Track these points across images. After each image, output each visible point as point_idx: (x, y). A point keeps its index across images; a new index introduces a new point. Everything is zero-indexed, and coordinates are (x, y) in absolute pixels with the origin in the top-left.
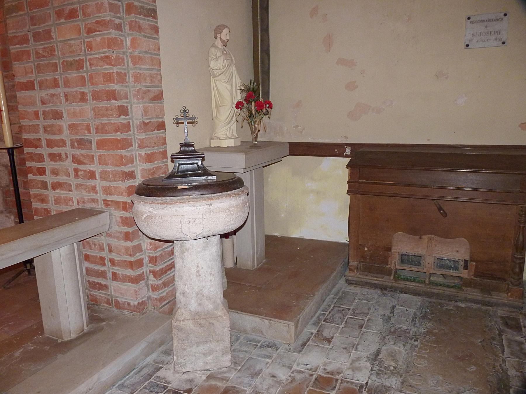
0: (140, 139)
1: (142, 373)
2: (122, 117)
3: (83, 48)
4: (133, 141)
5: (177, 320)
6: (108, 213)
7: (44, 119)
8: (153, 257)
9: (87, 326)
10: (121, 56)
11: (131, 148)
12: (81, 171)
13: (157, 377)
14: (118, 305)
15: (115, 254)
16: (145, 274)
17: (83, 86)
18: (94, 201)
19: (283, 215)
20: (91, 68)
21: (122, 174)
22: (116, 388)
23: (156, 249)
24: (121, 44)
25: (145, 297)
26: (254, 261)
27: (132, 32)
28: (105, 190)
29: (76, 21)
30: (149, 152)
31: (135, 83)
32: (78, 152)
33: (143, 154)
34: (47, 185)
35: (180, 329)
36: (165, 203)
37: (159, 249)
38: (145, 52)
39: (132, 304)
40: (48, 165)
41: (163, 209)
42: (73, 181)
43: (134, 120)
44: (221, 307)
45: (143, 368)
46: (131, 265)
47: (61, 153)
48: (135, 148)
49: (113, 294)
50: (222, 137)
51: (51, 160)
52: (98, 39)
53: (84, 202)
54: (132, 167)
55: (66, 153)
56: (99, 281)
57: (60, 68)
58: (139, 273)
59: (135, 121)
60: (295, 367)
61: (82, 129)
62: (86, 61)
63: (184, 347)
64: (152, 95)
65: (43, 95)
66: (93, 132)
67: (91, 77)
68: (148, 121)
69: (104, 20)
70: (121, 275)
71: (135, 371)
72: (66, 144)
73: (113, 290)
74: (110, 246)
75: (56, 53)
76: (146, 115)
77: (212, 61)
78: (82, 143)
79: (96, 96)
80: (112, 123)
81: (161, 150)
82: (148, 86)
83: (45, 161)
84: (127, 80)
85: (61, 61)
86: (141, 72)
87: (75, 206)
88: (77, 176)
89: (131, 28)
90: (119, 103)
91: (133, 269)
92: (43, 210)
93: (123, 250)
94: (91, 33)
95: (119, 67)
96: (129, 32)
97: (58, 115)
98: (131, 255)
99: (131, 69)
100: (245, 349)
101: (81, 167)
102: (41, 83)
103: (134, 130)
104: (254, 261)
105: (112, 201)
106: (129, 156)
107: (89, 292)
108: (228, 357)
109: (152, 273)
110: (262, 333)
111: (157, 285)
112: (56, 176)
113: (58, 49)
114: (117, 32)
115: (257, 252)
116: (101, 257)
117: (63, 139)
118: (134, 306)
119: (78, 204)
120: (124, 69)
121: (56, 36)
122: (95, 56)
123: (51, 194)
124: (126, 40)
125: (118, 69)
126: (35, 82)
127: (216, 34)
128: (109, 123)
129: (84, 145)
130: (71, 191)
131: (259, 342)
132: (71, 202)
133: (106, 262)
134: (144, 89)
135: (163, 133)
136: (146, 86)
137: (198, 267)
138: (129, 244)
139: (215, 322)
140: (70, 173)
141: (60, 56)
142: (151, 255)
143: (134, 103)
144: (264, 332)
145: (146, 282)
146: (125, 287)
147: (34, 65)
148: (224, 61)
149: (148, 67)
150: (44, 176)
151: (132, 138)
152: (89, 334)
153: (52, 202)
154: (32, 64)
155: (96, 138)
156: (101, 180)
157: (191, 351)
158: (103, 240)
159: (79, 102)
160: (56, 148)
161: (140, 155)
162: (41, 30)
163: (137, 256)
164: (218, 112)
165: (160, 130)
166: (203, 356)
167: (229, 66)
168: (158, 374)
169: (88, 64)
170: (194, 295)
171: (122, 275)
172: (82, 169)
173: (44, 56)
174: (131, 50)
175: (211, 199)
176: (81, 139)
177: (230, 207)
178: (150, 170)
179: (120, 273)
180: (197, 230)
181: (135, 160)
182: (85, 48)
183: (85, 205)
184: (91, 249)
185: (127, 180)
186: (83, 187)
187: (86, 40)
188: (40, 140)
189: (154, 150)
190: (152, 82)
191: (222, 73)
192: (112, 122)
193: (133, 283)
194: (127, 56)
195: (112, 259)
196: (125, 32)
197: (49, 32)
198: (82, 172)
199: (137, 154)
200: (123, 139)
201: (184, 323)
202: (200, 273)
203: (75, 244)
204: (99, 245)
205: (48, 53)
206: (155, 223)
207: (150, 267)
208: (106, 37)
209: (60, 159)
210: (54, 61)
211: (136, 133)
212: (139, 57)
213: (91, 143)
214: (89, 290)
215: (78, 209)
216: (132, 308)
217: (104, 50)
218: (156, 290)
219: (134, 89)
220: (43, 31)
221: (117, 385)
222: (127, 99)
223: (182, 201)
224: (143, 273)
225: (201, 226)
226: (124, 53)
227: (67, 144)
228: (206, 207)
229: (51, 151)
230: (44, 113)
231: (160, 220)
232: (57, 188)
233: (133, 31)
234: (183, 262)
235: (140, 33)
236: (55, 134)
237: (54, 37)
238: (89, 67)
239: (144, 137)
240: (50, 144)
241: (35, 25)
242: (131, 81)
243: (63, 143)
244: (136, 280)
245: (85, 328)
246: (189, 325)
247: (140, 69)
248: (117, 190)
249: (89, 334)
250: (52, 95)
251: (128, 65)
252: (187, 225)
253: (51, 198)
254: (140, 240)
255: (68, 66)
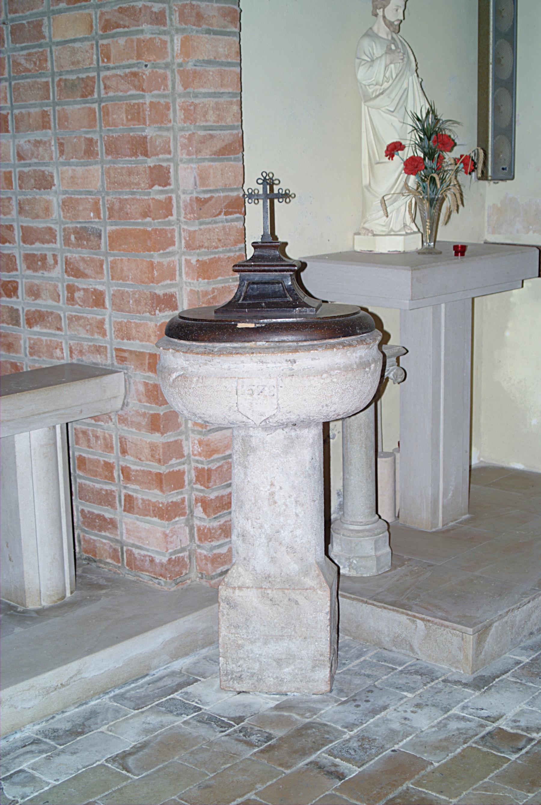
0: (190, 232)
1: (160, 684)
2: (156, 187)
3: (95, 57)
4: (176, 234)
5: (227, 585)
6: (122, 373)
7: (21, 187)
8: (203, 469)
9: (72, 593)
10: (161, 71)
11: (170, 249)
12: (79, 290)
13: (186, 693)
14: (133, 563)
15: (132, 459)
16: (186, 503)
17: (91, 127)
18: (99, 350)
19: (534, 421)
20: (107, 93)
21: (152, 299)
22: (110, 698)
23: (211, 455)
24: (161, 50)
25: (183, 550)
26: (435, 512)
27: (184, 26)
28: (120, 330)
29: (86, 7)
30: (205, 258)
31: (185, 122)
32: (75, 255)
33: (193, 261)
34: (18, 316)
35: (232, 605)
36: (209, 353)
37: (215, 456)
38: (209, 62)
39: (157, 561)
40: (23, 276)
41: (206, 364)
42: (64, 310)
43: (180, 192)
44: (315, 571)
45: (164, 677)
46: (159, 480)
47: (46, 255)
48: (180, 248)
49: (124, 538)
50: (378, 229)
51: (28, 268)
52: (122, 41)
53: (81, 352)
54: (171, 286)
55: (54, 256)
56: (102, 513)
57: (54, 93)
58: (174, 500)
59: (182, 196)
60: (456, 711)
61: (85, 209)
62: (99, 81)
63: (240, 642)
64: (218, 145)
65: (22, 142)
66: (105, 216)
67: (106, 112)
68: (207, 196)
69: (133, 7)
70: (140, 501)
71: (147, 679)
72: (55, 239)
73: (124, 531)
74: (123, 442)
75: (49, 64)
76: (203, 184)
77: (361, 68)
78: (84, 236)
79: (112, 148)
80: (137, 200)
81: (232, 254)
82: (211, 128)
83: (17, 270)
84: (171, 116)
85: (57, 79)
86: (197, 101)
87: (66, 359)
88: (71, 300)
89: (183, 18)
90: (151, 162)
91: (162, 490)
92: (9, 366)
93: (147, 451)
94: (110, 30)
95: (156, 92)
96: (178, 26)
97: (44, 182)
98: (159, 461)
99: (180, 96)
100: (368, 672)
101: (80, 283)
102: (18, 120)
103: (179, 214)
104: (435, 512)
105: (131, 352)
106: (165, 264)
107: (82, 535)
108: (324, 673)
109: (199, 504)
110: (412, 649)
111: (209, 529)
112: (36, 299)
113: (52, 57)
114: (155, 27)
115: (445, 494)
116: (106, 463)
117: (50, 229)
118: (162, 565)
119: (71, 357)
120: (165, 96)
121: (50, 32)
122: (113, 72)
123: (25, 335)
124: (172, 41)
125: (153, 96)
126: (9, 117)
127: (375, 7)
128: (133, 199)
129: (88, 240)
130: (59, 329)
131: (400, 665)
132: (58, 351)
133: (115, 475)
134: (202, 133)
135: (237, 219)
136: (205, 128)
137: (272, 485)
138: (157, 438)
139: (302, 601)
140: (61, 293)
141: (56, 70)
142: (200, 466)
143: (181, 160)
144: (416, 646)
145: (187, 520)
146: (147, 526)
147: (10, 84)
148: (386, 66)
149: (212, 90)
150: (14, 299)
151: (173, 230)
152: (72, 605)
153: (25, 348)
154: (7, 84)
155: (109, 228)
156: (113, 310)
157: (252, 652)
158: (112, 429)
159: (82, 158)
160: (38, 245)
161: (188, 262)
162: (24, 22)
163: (172, 465)
164: (373, 176)
165: (231, 213)
166: (275, 664)
167: (400, 75)
168: (189, 689)
169: (102, 86)
170: (263, 540)
171: (143, 500)
172: (80, 286)
173: (27, 70)
174: (180, 60)
175: (296, 350)
176: (82, 228)
177: (333, 369)
178: (206, 294)
179: (139, 496)
180: (265, 408)
181: (177, 273)
182: (97, 55)
183: (84, 358)
184: (89, 447)
185: (160, 311)
186: (81, 322)
187: (101, 42)
188: (10, 228)
189: (216, 253)
190: (220, 118)
191: (382, 93)
192: (138, 197)
193: (161, 517)
194: (173, 71)
195: (127, 467)
196: (172, 25)
197: (38, 25)
198: (82, 293)
199: (183, 262)
200: (157, 230)
201: (240, 594)
202: (276, 497)
203: (58, 428)
204: (105, 439)
205: (35, 64)
206: (191, 391)
207: (197, 490)
208: (134, 37)
209: (44, 267)
210: (44, 80)
211: (182, 219)
212: (195, 72)
213: (100, 236)
214: (84, 531)
215: (72, 364)
216: (158, 569)
217: (131, 61)
218: (206, 539)
219: (182, 133)
220: (28, 23)
221: (112, 694)
222: (169, 153)
223: (240, 351)
224: (183, 500)
225: (275, 401)
226: (167, 66)
227: (58, 238)
228: (285, 366)
229: (29, 249)
230: (22, 177)
231: (200, 385)
232: (37, 323)
233: (186, 24)
234: (246, 474)
235: (199, 26)
236: (37, 216)
237: (47, 34)
238: (103, 92)
239: (196, 228)
240: (29, 236)
241: (16, 12)
242: (178, 119)
243: (48, 235)
244: (168, 512)
245: (68, 594)
246: (250, 598)
247: (196, 96)
248: (141, 329)
249: (72, 605)
250: (38, 143)
251: (173, 88)
252: (248, 397)
253: (25, 342)
254: (180, 434)
255: (69, 88)
